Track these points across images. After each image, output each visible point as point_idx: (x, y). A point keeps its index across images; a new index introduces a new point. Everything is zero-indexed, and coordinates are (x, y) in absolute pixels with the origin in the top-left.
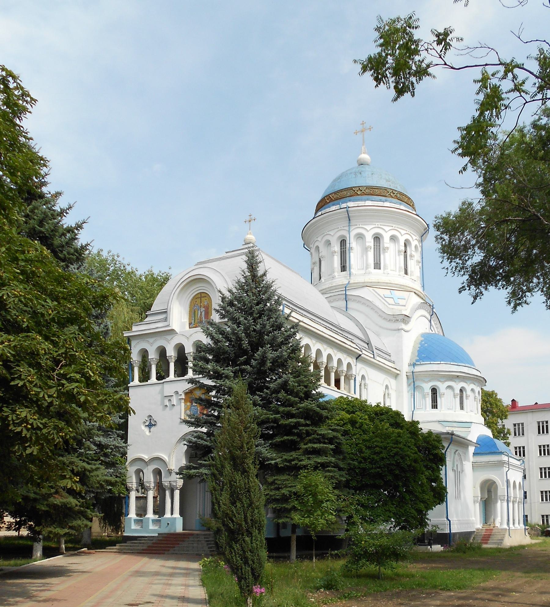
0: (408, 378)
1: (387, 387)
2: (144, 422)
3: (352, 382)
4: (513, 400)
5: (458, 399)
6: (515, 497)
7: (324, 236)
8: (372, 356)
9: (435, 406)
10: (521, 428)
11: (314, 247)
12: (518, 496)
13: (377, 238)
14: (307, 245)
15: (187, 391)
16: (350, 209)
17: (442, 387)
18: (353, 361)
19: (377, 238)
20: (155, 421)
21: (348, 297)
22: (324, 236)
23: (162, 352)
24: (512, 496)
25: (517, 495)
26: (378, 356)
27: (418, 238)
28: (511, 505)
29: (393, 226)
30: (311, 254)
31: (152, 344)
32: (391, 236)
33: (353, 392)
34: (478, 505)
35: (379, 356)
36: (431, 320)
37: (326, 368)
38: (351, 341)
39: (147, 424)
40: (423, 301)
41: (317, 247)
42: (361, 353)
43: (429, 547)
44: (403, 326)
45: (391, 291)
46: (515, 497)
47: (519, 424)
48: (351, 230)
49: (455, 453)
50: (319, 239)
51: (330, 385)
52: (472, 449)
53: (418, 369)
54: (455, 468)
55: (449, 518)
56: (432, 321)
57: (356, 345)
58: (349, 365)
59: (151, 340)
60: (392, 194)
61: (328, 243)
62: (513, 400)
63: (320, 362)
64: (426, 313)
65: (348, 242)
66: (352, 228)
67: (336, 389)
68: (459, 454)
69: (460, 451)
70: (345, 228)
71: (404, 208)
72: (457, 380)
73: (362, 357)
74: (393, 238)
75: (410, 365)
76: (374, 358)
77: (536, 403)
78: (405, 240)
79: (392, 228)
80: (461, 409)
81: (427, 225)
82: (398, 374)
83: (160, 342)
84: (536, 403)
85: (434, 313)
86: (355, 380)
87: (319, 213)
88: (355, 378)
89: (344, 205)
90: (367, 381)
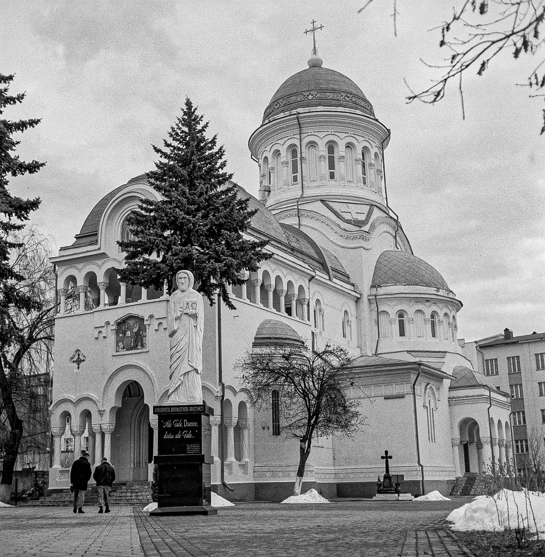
0: (370, 303)
1: (346, 312)
2: (72, 358)
3: (305, 307)
4: (506, 330)
5: (429, 326)
6: (501, 440)
7: (273, 145)
8: (328, 278)
9: (402, 333)
10: (516, 362)
11: (263, 158)
12: (505, 438)
13: (331, 147)
14: (254, 154)
15: (119, 321)
16: (300, 115)
17: (410, 309)
18: (305, 283)
19: (331, 147)
20: (84, 356)
21: (301, 212)
22: (273, 145)
23: (91, 278)
24: (497, 437)
25: (503, 437)
26: (335, 278)
27: (378, 144)
28: (496, 448)
29: (348, 133)
30: (260, 166)
31: (80, 270)
32: (347, 144)
33: (306, 319)
34: (456, 449)
35: (335, 277)
36: (396, 236)
37: (262, 286)
38: (303, 262)
39: (75, 359)
40: (386, 215)
41: (266, 158)
42: (314, 274)
43: (397, 495)
44: (362, 243)
45: (349, 204)
46: (501, 440)
47: (513, 358)
48: (302, 138)
49: (426, 389)
50: (268, 149)
51: (268, 307)
52: (447, 383)
53: (381, 291)
54: (427, 405)
55: (421, 463)
56: (397, 237)
57: (309, 266)
58: (301, 288)
59: (80, 266)
60: (346, 98)
61: (277, 153)
62: (506, 330)
63: (268, 285)
64: (390, 228)
65: (299, 151)
66: (303, 136)
67: (274, 311)
68: (431, 388)
69: (433, 384)
70: (295, 136)
71: (361, 113)
72: (428, 304)
73: (316, 279)
74: (349, 146)
75: (372, 287)
76: (330, 280)
77: (534, 333)
78: (363, 148)
79: (347, 135)
80: (433, 336)
81: (388, 130)
82: (358, 298)
83: (91, 268)
84: (534, 333)
85: (399, 228)
86: (308, 305)
87: (267, 121)
88: (309, 303)
89: (294, 112)
90: (323, 307)
